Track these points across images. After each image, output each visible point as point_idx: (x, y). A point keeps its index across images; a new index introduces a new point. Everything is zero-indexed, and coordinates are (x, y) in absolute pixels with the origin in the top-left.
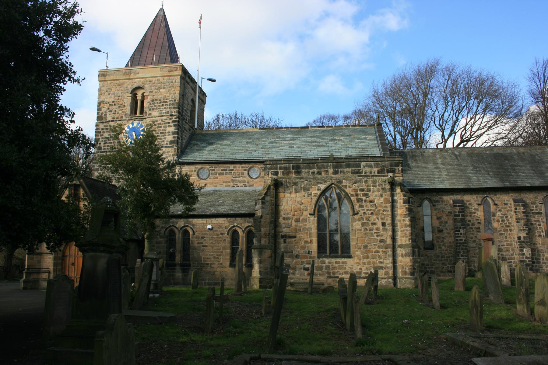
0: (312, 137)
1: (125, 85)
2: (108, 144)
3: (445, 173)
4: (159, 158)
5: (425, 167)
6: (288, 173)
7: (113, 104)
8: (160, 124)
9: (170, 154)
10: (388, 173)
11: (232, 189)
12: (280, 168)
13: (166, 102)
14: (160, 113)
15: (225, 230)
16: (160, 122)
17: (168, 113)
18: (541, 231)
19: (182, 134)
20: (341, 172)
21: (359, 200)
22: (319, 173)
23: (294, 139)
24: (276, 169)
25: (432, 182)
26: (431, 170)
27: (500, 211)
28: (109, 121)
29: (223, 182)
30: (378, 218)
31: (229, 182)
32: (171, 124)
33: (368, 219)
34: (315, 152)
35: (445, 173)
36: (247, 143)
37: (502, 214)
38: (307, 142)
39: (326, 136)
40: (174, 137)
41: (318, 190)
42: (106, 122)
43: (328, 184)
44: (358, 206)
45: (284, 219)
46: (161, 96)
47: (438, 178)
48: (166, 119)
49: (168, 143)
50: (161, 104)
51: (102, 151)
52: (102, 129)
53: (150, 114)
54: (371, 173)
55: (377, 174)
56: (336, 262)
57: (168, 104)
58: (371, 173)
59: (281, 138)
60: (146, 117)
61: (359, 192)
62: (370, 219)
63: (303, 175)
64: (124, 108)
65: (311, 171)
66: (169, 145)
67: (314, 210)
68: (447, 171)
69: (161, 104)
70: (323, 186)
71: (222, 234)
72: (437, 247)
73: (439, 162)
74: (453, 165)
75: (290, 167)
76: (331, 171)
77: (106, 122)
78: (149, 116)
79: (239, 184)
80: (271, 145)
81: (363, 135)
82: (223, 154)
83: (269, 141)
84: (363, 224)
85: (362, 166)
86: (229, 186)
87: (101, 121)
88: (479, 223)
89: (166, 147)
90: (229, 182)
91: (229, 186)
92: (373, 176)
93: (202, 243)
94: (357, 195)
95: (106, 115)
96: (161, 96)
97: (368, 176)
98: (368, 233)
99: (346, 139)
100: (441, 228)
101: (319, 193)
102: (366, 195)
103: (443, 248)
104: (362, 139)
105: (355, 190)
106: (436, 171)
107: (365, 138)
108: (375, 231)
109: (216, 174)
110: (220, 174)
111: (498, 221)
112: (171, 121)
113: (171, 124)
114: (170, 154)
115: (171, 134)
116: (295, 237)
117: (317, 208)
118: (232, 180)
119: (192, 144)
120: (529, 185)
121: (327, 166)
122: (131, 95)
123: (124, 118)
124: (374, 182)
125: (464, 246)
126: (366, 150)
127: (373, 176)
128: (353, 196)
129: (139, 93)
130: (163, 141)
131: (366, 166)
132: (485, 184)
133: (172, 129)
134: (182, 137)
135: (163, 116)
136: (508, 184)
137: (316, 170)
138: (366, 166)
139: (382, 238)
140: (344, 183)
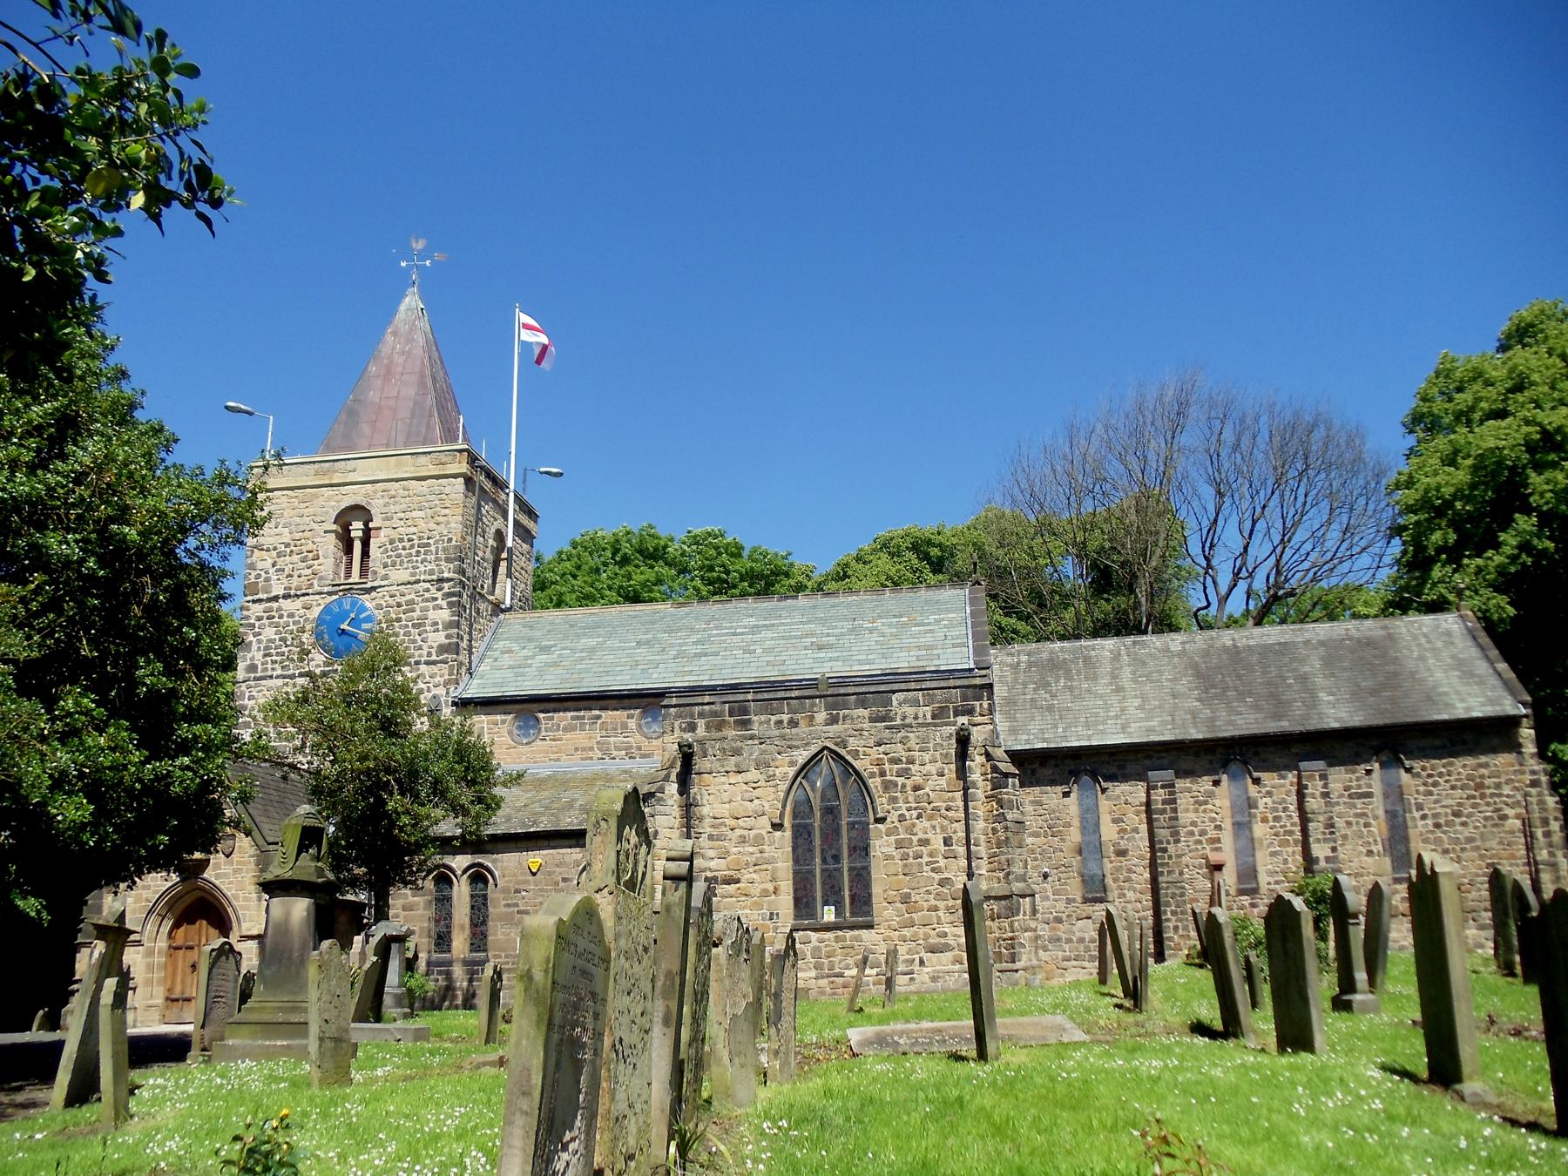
0: (802, 623)
1: (321, 501)
2: (274, 658)
3: (1137, 702)
4: (406, 699)
5: (1089, 691)
6: (720, 726)
7: (288, 550)
8: (411, 602)
9: (437, 679)
10: (956, 715)
11: (597, 767)
12: (701, 715)
13: (428, 545)
14: (413, 575)
15: (573, 871)
16: (413, 596)
17: (431, 572)
18: (1371, 840)
19: (471, 626)
20: (845, 717)
21: (888, 786)
22: (793, 723)
23: (755, 629)
24: (692, 716)
25: (1101, 727)
26: (1101, 696)
27: (1269, 794)
28: (276, 598)
29: (576, 749)
30: (934, 827)
31: (591, 749)
32: (439, 602)
33: (910, 830)
34: (808, 663)
35: (1137, 702)
36: (639, 644)
37: (1274, 802)
38: (791, 638)
39: (841, 620)
40: (448, 637)
41: (792, 764)
42: (269, 600)
43: (814, 749)
44: (884, 800)
45: (711, 837)
46: (413, 530)
47: (1117, 717)
48: (428, 590)
49: (433, 651)
50: (413, 551)
51: (259, 674)
52: (259, 619)
53: (385, 577)
54: (916, 718)
55: (930, 721)
56: (1137, 1024)
57: (433, 548)
58: (916, 718)
59: (726, 628)
60: (375, 584)
61: (887, 766)
62: (915, 830)
63: (756, 729)
64: (316, 562)
65: (773, 718)
66: (434, 657)
67: (782, 815)
68: (1143, 697)
69: (413, 551)
70: (802, 756)
71: (565, 880)
72: (1116, 893)
73: (1126, 673)
74: (1158, 681)
75: (724, 711)
76: (821, 716)
77: (269, 600)
78: (383, 583)
79: (615, 753)
80: (699, 650)
81: (934, 613)
82: (575, 676)
83: (694, 638)
84: (899, 845)
85: (895, 703)
86: (591, 758)
87: (256, 597)
88: (1218, 828)
89: (427, 663)
90: (591, 749)
91: (591, 758)
92: (921, 725)
93: (517, 905)
94: (883, 774)
95: (267, 580)
96: (413, 530)
97: (910, 726)
98: (911, 864)
99: (890, 625)
100: (1123, 844)
101: (792, 772)
102: (904, 773)
103: (1130, 895)
104: (929, 624)
105: (879, 763)
106: (1114, 700)
107: (938, 621)
108: (926, 859)
109: (558, 730)
110: (565, 730)
111: (1265, 820)
112: (439, 595)
113: (439, 602)
114: (437, 679)
115: (440, 627)
116: (738, 881)
117: (789, 808)
118: (598, 743)
119: (496, 650)
120: (1336, 725)
121: (814, 705)
122: (334, 527)
123: (317, 588)
124: (925, 740)
125: (1177, 888)
126: (935, 652)
127: (921, 725)
128: (872, 775)
129: (357, 528)
130: (420, 648)
131: (905, 701)
132: (1230, 728)
133: (445, 615)
134: (470, 634)
135: (417, 582)
136: (1286, 724)
137: (785, 717)
138: (905, 701)
139: (946, 875)
140: (853, 743)
